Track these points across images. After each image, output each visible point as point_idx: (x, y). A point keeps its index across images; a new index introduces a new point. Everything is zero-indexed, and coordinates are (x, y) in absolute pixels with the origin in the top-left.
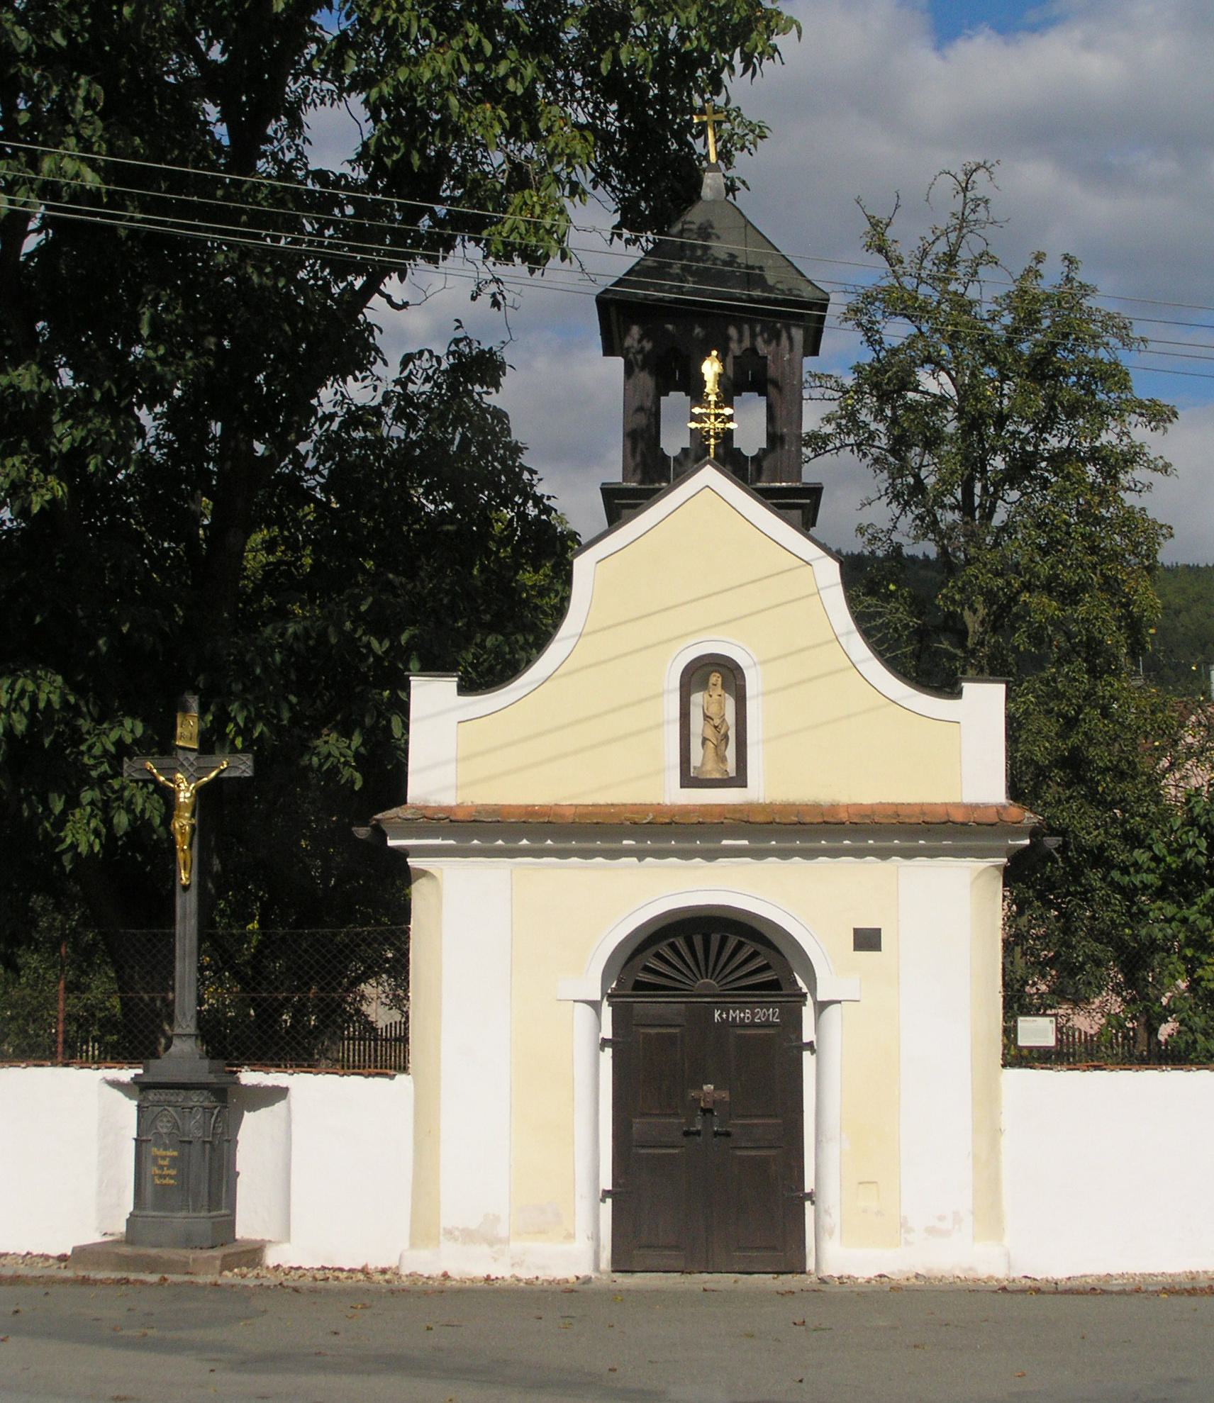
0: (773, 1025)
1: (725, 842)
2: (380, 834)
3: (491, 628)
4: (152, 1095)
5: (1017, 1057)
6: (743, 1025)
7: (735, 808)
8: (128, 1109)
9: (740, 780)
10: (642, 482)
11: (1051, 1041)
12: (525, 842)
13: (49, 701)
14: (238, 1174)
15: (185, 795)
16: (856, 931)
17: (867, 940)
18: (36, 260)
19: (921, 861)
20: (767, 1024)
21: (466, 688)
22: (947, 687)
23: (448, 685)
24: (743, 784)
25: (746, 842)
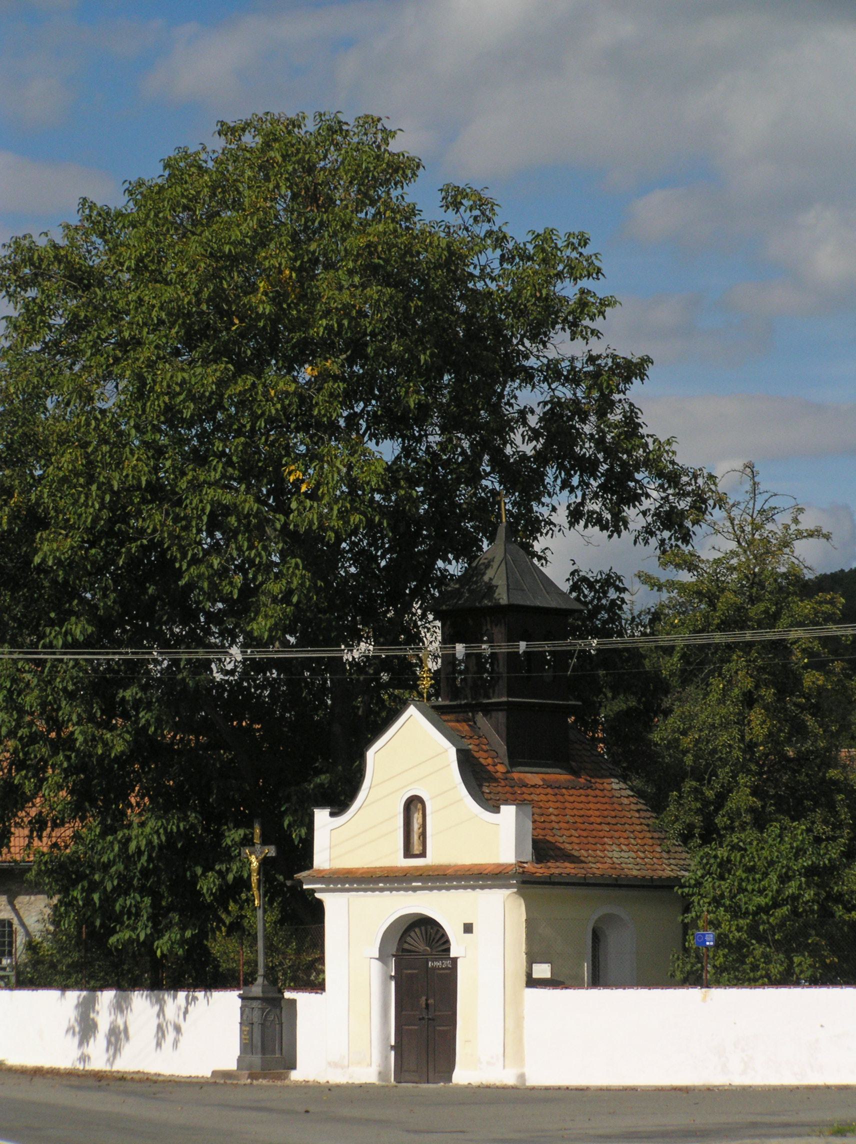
0: (449, 968)
1: (414, 884)
2: (301, 883)
3: (810, 714)
4: (248, 1003)
5: (532, 982)
6: (439, 969)
7: (417, 868)
8: (239, 1002)
9: (423, 854)
10: (473, 699)
11: (548, 975)
12: (347, 886)
13: (172, 829)
14: (77, 1007)
15: (255, 864)
16: (472, 924)
17: (468, 928)
18: (394, 556)
19: (487, 891)
20: (447, 968)
21: (332, 814)
22: (496, 809)
23: (327, 812)
24: (423, 854)
25: (420, 884)
